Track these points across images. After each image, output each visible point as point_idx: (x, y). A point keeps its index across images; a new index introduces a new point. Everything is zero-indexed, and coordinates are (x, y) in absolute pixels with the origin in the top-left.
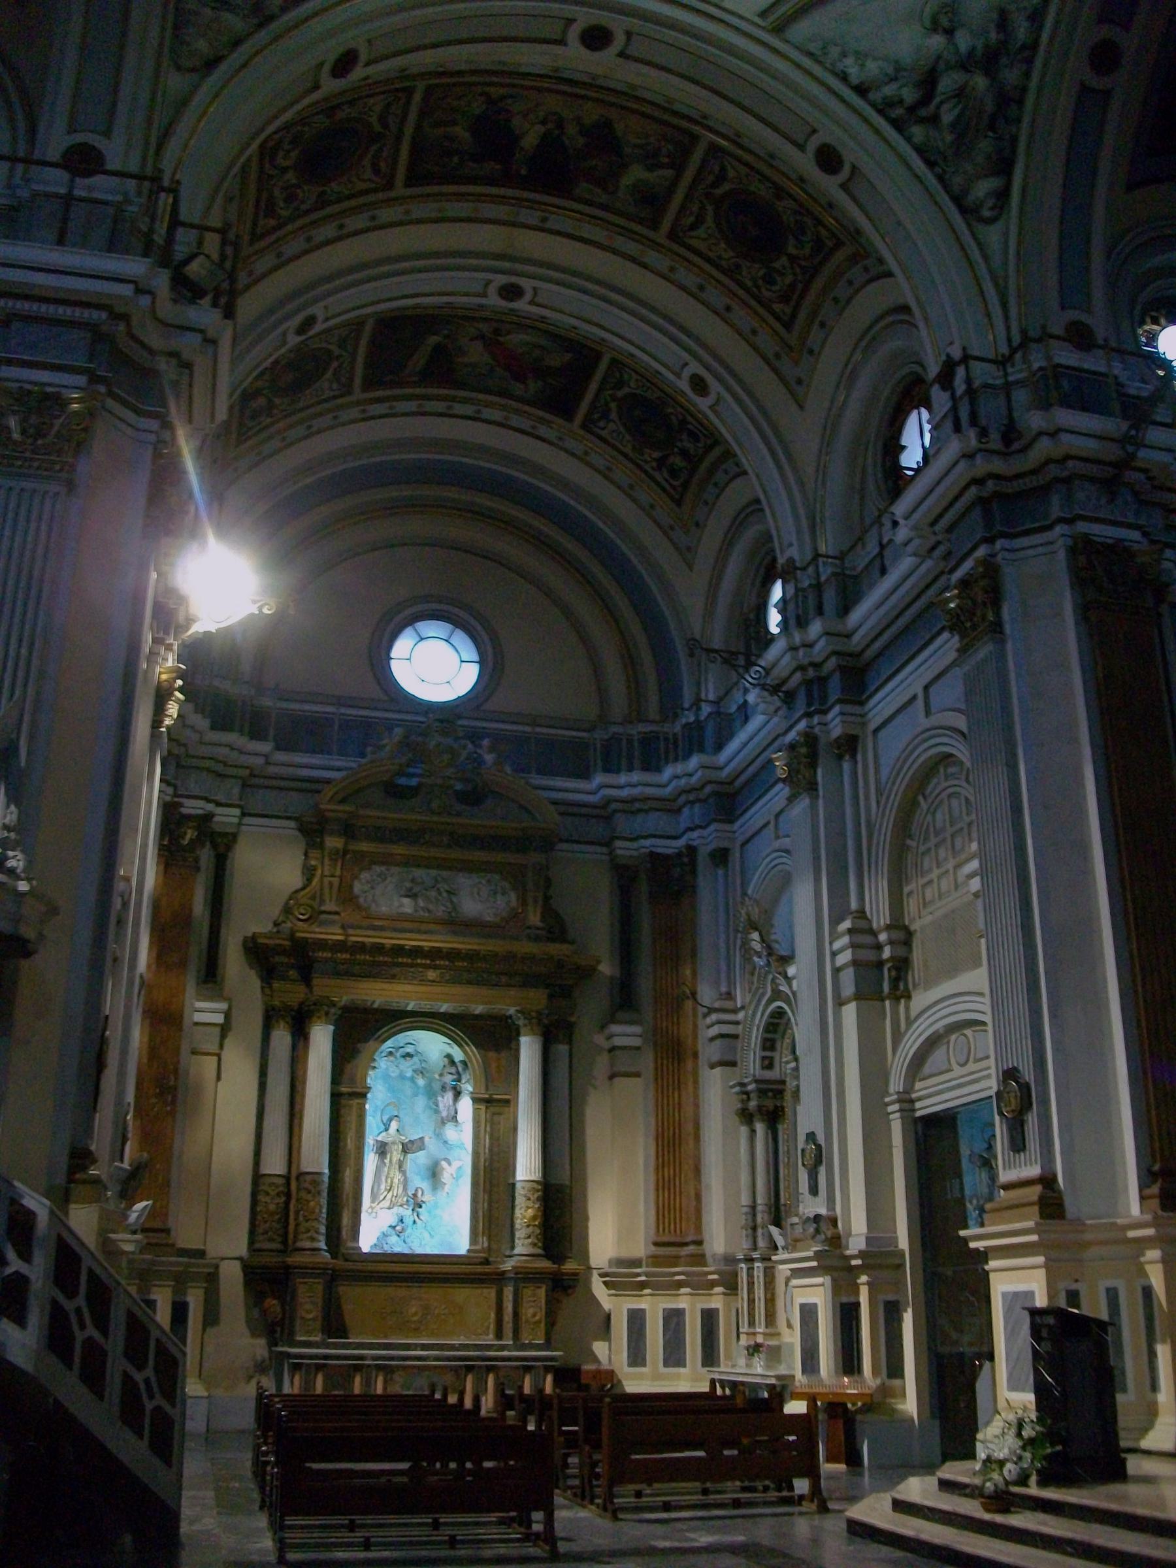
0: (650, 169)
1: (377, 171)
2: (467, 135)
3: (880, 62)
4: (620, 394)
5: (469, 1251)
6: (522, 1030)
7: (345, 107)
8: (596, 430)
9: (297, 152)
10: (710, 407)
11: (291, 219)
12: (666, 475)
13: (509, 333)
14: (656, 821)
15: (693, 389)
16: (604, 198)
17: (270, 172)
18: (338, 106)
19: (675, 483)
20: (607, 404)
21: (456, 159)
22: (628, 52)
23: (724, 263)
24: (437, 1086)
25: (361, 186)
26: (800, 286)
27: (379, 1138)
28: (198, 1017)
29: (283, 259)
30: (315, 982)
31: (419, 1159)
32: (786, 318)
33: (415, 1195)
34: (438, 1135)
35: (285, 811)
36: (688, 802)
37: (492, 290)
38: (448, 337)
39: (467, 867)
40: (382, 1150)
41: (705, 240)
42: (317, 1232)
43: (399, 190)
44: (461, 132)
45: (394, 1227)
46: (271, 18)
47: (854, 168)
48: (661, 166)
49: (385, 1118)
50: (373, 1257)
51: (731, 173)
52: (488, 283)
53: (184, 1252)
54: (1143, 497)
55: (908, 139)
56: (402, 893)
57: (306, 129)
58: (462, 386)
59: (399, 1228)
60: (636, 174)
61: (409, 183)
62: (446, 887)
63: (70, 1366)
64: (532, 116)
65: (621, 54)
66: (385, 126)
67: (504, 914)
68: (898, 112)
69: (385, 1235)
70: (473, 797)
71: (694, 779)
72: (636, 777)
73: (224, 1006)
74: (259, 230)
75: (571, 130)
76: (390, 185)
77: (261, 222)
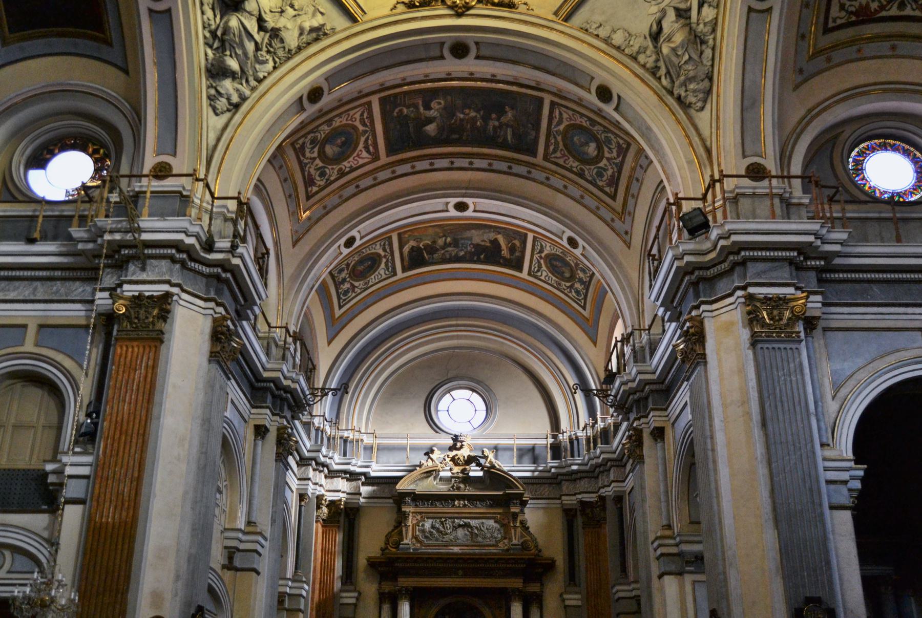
1: (368, 152)
9: (317, 148)
20: (539, 262)
23: (575, 169)
25: (361, 162)
29: (327, 209)
30: (399, 579)
37: (451, 207)
47: (619, 97)
52: (447, 203)
57: (317, 134)
73: (356, 594)
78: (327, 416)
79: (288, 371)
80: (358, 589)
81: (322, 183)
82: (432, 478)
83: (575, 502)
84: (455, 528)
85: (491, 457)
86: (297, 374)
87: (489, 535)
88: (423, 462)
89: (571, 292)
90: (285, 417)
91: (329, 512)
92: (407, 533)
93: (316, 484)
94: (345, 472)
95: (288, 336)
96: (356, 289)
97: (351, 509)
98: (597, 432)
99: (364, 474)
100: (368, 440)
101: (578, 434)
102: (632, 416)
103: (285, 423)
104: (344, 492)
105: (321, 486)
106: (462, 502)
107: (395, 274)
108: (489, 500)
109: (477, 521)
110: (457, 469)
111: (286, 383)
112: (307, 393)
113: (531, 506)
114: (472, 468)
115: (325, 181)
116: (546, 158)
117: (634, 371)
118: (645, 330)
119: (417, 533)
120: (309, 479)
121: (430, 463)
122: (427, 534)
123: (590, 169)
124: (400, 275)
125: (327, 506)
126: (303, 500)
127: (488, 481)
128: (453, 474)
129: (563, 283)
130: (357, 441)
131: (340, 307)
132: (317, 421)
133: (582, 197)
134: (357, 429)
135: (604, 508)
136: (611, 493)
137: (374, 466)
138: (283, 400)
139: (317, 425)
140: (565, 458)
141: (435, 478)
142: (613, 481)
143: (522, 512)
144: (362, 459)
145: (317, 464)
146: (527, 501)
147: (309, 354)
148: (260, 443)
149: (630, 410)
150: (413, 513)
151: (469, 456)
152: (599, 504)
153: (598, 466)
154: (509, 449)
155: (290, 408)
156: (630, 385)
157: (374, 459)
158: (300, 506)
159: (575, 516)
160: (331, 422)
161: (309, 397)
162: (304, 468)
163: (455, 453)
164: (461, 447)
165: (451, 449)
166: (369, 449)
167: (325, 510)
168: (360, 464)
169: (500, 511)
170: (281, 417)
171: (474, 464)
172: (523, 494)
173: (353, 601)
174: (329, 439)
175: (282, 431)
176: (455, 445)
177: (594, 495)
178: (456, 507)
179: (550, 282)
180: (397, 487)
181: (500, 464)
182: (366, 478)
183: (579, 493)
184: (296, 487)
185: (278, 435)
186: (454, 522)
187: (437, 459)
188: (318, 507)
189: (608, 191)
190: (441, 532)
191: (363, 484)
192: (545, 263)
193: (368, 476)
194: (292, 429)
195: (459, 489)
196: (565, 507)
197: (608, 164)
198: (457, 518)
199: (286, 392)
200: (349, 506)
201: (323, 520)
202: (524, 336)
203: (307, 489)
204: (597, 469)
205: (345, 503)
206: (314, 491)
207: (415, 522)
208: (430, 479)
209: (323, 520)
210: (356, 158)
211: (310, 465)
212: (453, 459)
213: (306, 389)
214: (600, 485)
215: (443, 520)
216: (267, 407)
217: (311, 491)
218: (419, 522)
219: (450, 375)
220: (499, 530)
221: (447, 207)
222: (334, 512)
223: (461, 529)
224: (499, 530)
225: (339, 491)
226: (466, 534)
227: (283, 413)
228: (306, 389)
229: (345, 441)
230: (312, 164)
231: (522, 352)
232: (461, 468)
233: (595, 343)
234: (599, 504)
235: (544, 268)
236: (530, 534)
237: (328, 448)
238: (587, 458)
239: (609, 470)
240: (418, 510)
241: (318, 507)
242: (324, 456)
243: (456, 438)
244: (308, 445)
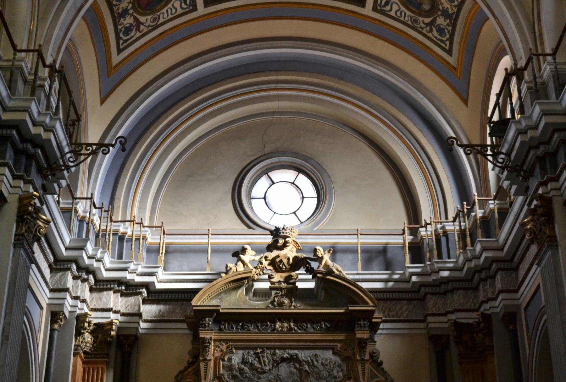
54: (514, 80)
78: (96, 199)
79: (39, 113)
82: (242, 291)
83: (446, 325)
84: (276, 363)
85: (327, 258)
86: (51, 118)
87: (325, 373)
88: (230, 265)
89: (431, 31)
90: (31, 182)
91: (94, 342)
92: (206, 371)
93: (76, 298)
94: (119, 282)
95: (41, 64)
96: (142, 27)
97: (127, 337)
98: (476, 220)
99: (146, 285)
100: (152, 238)
101: (447, 228)
102: (533, 183)
103: (31, 190)
104: (116, 312)
105: (84, 301)
106: (286, 325)
107: (195, 9)
108: (325, 321)
109: (308, 353)
110: (278, 277)
111: (34, 130)
112: (67, 150)
113: (384, 332)
114: (300, 277)
117: (537, 110)
119: (222, 371)
120: (67, 290)
121: (241, 268)
122: (235, 373)
124: (201, 10)
125: (92, 333)
126: (56, 322)
127: (323, 294)
128: (272, 283)
129: (421, 19)
130: (138, 239)
131: (119, 51)
132: (81, 207)
134: (137, 220)
135: (489, 333)
136: (498, 310)
137: (161, 274)
138: (31, 157)
139: (81, 213)
140: (430, 260)
141: (247, 291)
142: (501, 292)
143: (372, 339)
144: (144, 264)
145: (79, 268)
146: (378, 324)
147: (71, 96)
149: (529, 174)
150: (215, 340)
151: (295, 258)
152: (482, 325)
153: (477, 270)
154: (351, 250)
155: (40, 170)
156: (530, 133)
157: (162, 264)
158: (52, 330)
160: (101, 208)
161: (68, 155)
162: (59, 274)
163: (275, 253)
164: (285, 245)
165: (270, 248)
166: (153, 251)
167: (88, 338)
168: (140, 270)
169: (341, 337)
170: (26, 182)
171: (302, 271)
172: (372, 312)
174: (97, 236)
175: (26, 201)
176: (275, 242)
177: (475, 315)
178: (278, 332)
179: (402, 19)
180: (193, 302)
181: (340, 269)
182: (149, 292)
183: (452, 312)
184: (47, 301)
185: (19, 208)
186: (274, 354)
187: (250, 262)
188: (79, 333)
190: (256, 369)
191: (145, 301)
193: (151, 288)
194: (42, 204)
195: (281, 305)
198: (280, 348)
199: (35, 146)
200: (123, 333)
201: (85, 353)
202: (366, 95)
203: (62, 305)
204: (477, 276)
205: (119, 328)
206: (73, 309)
207: (217, 354)
208: (240, 291)
209: (85, 353)
211: (69, 269)
212: (273, 262)
213: (64, 143)
214: (481, 298)
215: (259, 351)
217: (69, 309)
218: (224, 354)
219: (267, 150)
220: (339, 366)
222: (101, 342)
223: (284, 364)
224: (339, 366)
225: (109, 310)
226: (292, 373)
227: (28, 175)
228: (64, 143)
229: (122, 238)
231: (364, 117)
232: (285, 275)
233: (466, 102)
234: (482, 325)
236: (384, 372)
237: (96, 245)
238: (461, 259)
239: (494, 277)
240: (223, 336)
241: (79, 333)
242: (89, 257)
243: (276, 233)
244: (67, 240)
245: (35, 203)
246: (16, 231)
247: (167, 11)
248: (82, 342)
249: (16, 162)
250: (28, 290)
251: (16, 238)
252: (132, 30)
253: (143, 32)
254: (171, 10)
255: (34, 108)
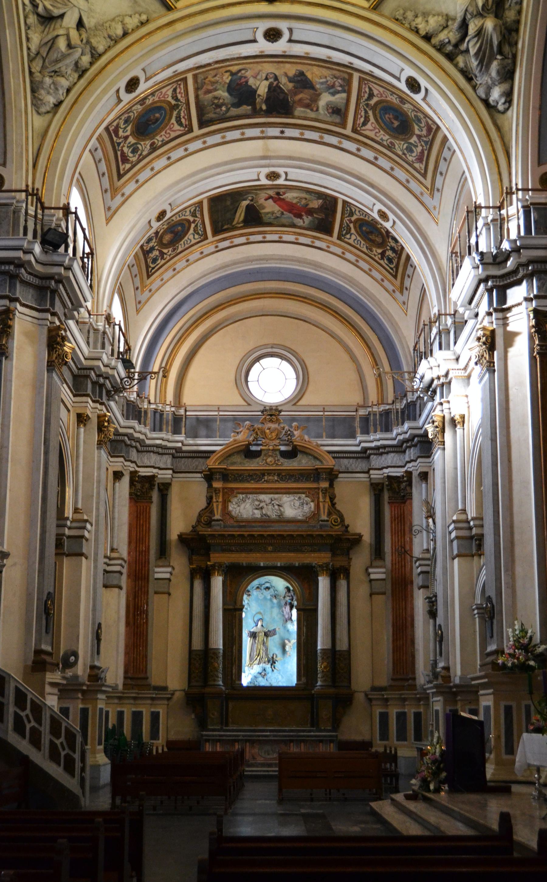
0: (333, 94)
1: (180, 124)
2: (226, 94)
3: (436, 17)
4: (353, 219)
5: (296, 684)
6: (319, 573)
7: (150, 97)
8: (346, 240)
10: (391, 227)
11: (139, 161)
12: (386, 261)
13: (284, 193)
14: (391, 458)
15: (380, 218)
16: (312, 115)
17: (118, 141)
18: (145, 98)
19: (392, 266)
20: (348, 225)
21: (224, 108)
22: (293, 38)
23: (385, 143)
24: (283, 602)
25: (173, 135)
26: (426, 152)
27: (252, 630)
28: (157, 576)
30: (211, 555)
31: (276, 639)
32: (423, 172)
33: (273, 658)
34: (285, 627)
35: (196, 469)
36: (407, 447)
38: (252, 200)
39: (288, 491)
40: (253, 635)
41: (371, 130)
42: (218, 677)
43: (197, 131)
44: (223, 94)
45: (261, 674)
46: (85, 71)
48: (339, 92)
49: (256, 619)
50: (248, 687)
51: (376, 92)
53: (156, 688)
55: (456, 66)
56: (254, 507)
57: (131, 114)
58: (270, 224)
59: (263, 674)
60: (325, 99)
61: (201, 126)
62: (277, 503)
63: (24, 737)
64: (259, 77)
65: (290, 41)
66: (177, 99)
67: (308, 515)
68: (449, 48)
69: (256, 677)
70: (292, 454)
71: (407, 436)
72: (378, 436)
74: (122, 172)
75: (283, 80)
76: (191, 130)
77: (121, 167)
80: (171, 564)
81: (134, 159)
96: (165, 256)
103: (58, 323)
115: (137, 156)
116: (354, 130)
118: (450, 315)
123: (400, 144)
133: (392, 169)
145: (98, 376)
148: (82, 430)
152: (405, 479)
159: (382, 490)
173: (167, 576)
175: (54, 333)
189: (419, 168)
192: (355, 227)
194: (65, 331)
196: (373, 481)
197: (417, 141)
210: (168, 131)
214: (407, 459)
216: (122, 456)
221: (258, 176)
230: (125, 143)
234: (405, 479)
235: (353, 231)
242: (105, 366)
245: (62, 334)
246: (98, 437)
247: (184, 242)
248: (104, 438)
249: (93, 391)
250: (62, 404)
251: (49, 364)
252: (158, 260)
253: (167, 260)
254: (187, 241)
255: (105, 358)
